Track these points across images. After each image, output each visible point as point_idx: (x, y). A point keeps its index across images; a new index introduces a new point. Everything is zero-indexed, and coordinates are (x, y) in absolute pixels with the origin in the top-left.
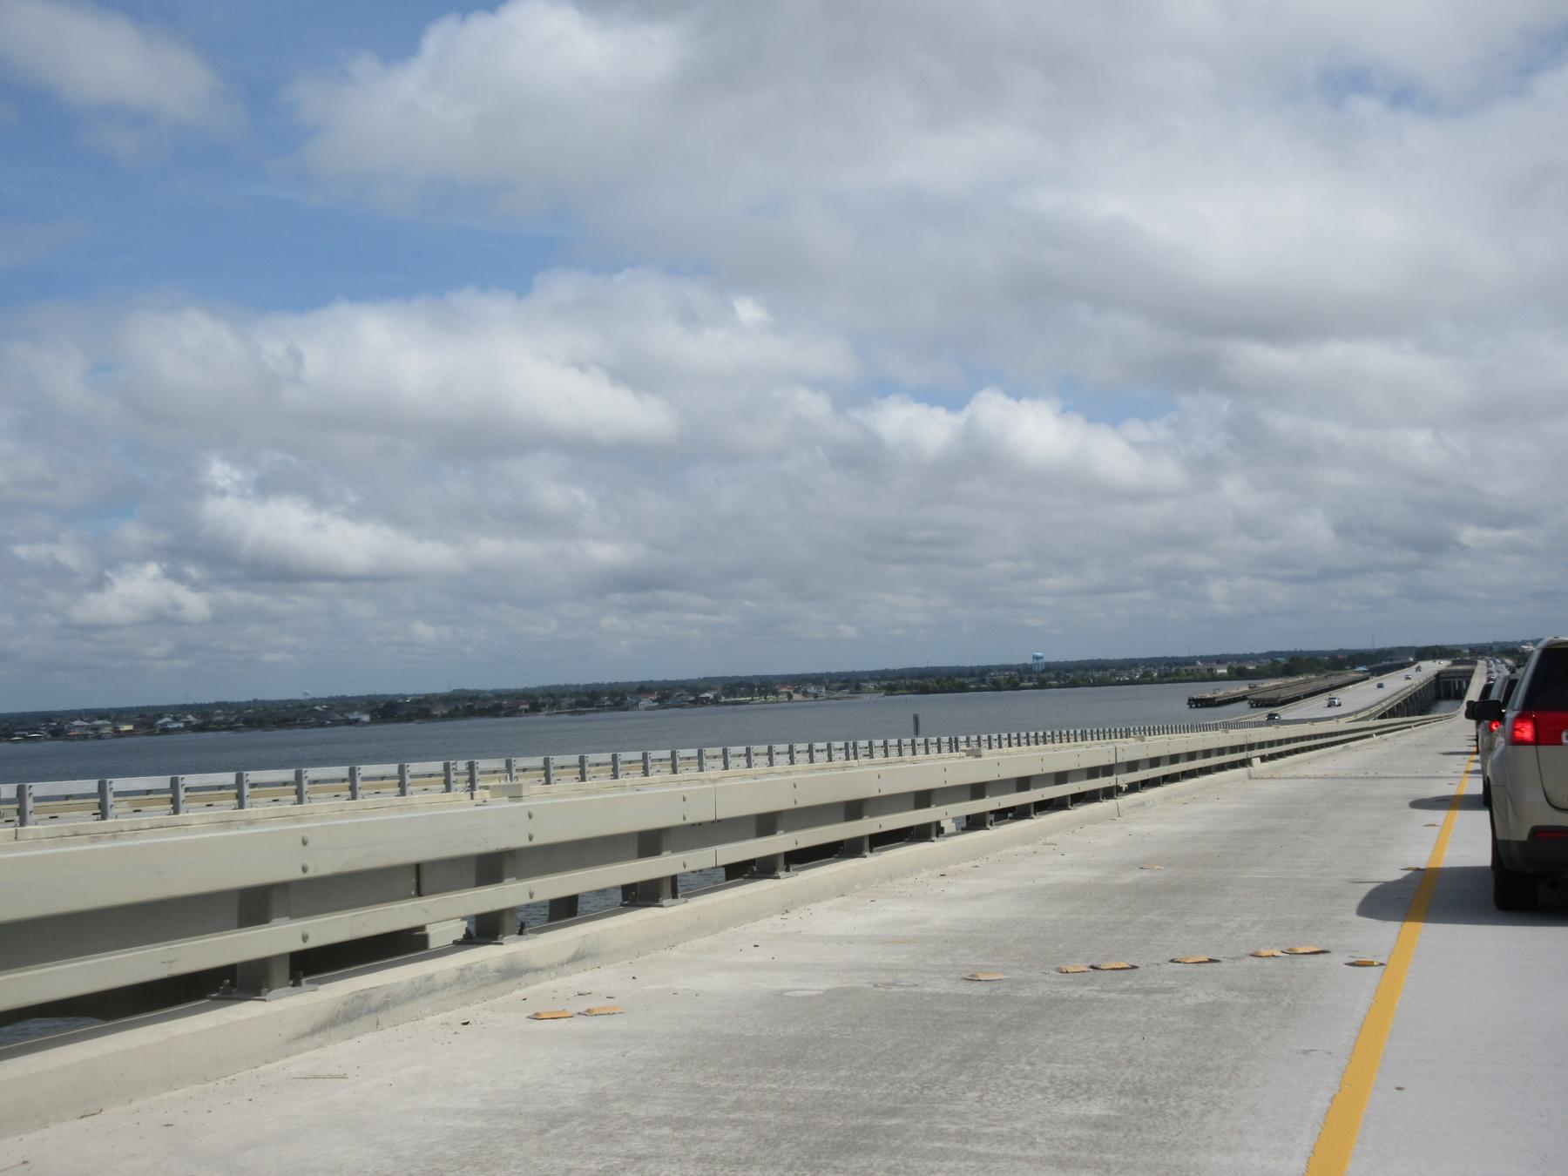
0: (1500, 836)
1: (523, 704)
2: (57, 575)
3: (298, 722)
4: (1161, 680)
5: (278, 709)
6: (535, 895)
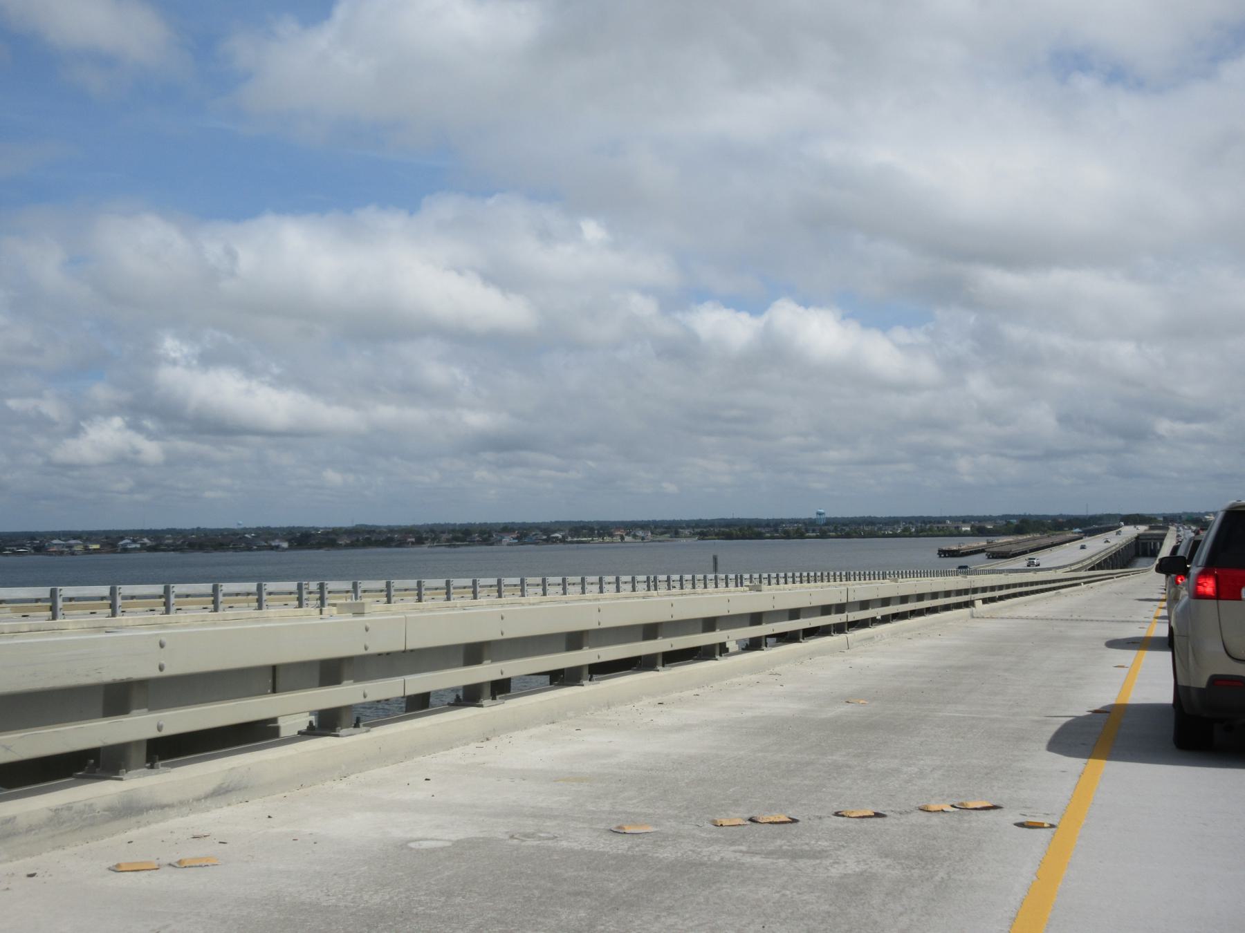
0: (1182, 682)
1: (410, 538)
2: (41, 424)
3: (231, 546)
4: (918, 534)
5: (216, 535)
6: (164, 728)
